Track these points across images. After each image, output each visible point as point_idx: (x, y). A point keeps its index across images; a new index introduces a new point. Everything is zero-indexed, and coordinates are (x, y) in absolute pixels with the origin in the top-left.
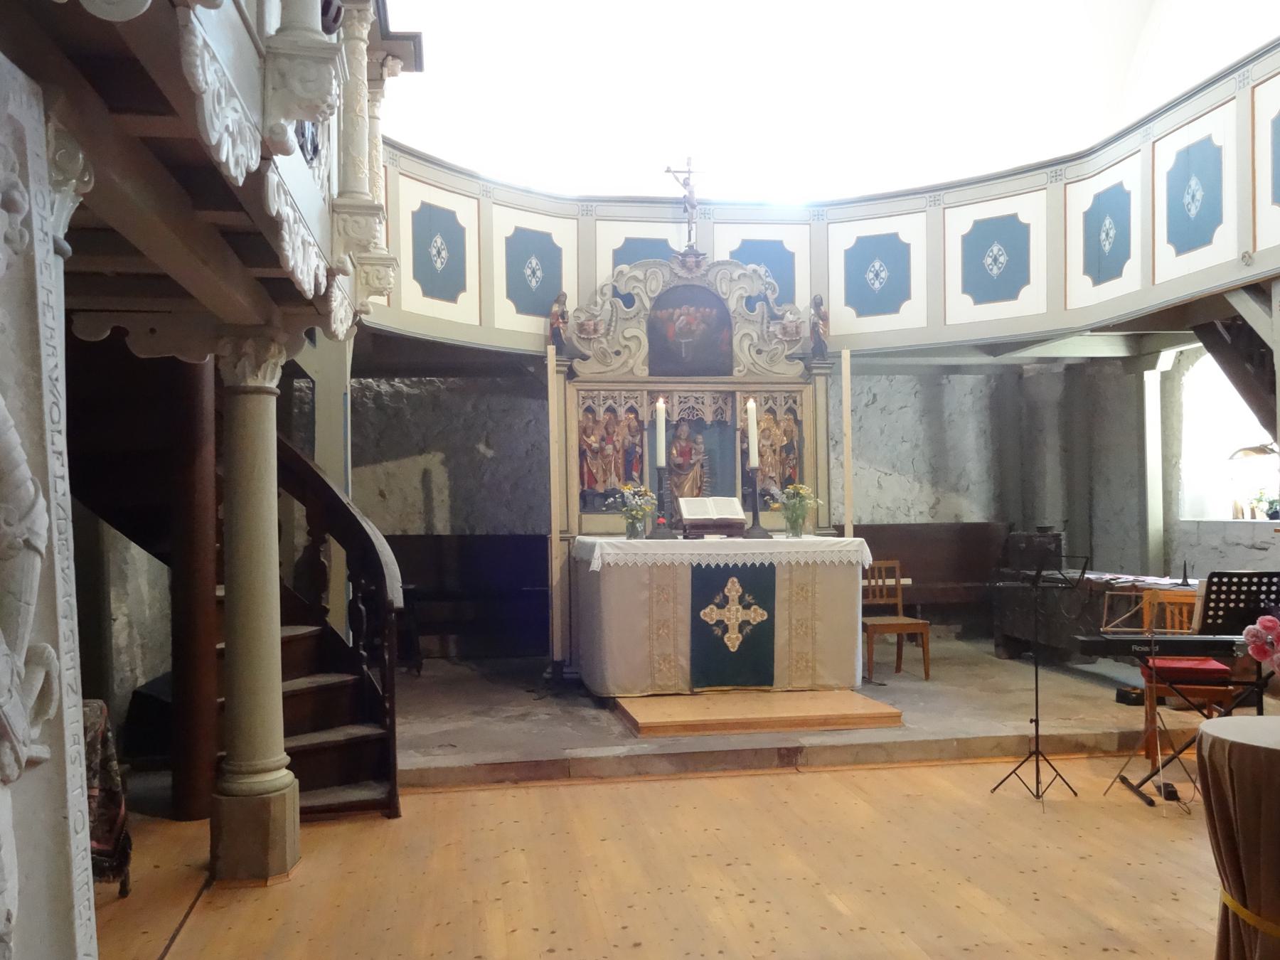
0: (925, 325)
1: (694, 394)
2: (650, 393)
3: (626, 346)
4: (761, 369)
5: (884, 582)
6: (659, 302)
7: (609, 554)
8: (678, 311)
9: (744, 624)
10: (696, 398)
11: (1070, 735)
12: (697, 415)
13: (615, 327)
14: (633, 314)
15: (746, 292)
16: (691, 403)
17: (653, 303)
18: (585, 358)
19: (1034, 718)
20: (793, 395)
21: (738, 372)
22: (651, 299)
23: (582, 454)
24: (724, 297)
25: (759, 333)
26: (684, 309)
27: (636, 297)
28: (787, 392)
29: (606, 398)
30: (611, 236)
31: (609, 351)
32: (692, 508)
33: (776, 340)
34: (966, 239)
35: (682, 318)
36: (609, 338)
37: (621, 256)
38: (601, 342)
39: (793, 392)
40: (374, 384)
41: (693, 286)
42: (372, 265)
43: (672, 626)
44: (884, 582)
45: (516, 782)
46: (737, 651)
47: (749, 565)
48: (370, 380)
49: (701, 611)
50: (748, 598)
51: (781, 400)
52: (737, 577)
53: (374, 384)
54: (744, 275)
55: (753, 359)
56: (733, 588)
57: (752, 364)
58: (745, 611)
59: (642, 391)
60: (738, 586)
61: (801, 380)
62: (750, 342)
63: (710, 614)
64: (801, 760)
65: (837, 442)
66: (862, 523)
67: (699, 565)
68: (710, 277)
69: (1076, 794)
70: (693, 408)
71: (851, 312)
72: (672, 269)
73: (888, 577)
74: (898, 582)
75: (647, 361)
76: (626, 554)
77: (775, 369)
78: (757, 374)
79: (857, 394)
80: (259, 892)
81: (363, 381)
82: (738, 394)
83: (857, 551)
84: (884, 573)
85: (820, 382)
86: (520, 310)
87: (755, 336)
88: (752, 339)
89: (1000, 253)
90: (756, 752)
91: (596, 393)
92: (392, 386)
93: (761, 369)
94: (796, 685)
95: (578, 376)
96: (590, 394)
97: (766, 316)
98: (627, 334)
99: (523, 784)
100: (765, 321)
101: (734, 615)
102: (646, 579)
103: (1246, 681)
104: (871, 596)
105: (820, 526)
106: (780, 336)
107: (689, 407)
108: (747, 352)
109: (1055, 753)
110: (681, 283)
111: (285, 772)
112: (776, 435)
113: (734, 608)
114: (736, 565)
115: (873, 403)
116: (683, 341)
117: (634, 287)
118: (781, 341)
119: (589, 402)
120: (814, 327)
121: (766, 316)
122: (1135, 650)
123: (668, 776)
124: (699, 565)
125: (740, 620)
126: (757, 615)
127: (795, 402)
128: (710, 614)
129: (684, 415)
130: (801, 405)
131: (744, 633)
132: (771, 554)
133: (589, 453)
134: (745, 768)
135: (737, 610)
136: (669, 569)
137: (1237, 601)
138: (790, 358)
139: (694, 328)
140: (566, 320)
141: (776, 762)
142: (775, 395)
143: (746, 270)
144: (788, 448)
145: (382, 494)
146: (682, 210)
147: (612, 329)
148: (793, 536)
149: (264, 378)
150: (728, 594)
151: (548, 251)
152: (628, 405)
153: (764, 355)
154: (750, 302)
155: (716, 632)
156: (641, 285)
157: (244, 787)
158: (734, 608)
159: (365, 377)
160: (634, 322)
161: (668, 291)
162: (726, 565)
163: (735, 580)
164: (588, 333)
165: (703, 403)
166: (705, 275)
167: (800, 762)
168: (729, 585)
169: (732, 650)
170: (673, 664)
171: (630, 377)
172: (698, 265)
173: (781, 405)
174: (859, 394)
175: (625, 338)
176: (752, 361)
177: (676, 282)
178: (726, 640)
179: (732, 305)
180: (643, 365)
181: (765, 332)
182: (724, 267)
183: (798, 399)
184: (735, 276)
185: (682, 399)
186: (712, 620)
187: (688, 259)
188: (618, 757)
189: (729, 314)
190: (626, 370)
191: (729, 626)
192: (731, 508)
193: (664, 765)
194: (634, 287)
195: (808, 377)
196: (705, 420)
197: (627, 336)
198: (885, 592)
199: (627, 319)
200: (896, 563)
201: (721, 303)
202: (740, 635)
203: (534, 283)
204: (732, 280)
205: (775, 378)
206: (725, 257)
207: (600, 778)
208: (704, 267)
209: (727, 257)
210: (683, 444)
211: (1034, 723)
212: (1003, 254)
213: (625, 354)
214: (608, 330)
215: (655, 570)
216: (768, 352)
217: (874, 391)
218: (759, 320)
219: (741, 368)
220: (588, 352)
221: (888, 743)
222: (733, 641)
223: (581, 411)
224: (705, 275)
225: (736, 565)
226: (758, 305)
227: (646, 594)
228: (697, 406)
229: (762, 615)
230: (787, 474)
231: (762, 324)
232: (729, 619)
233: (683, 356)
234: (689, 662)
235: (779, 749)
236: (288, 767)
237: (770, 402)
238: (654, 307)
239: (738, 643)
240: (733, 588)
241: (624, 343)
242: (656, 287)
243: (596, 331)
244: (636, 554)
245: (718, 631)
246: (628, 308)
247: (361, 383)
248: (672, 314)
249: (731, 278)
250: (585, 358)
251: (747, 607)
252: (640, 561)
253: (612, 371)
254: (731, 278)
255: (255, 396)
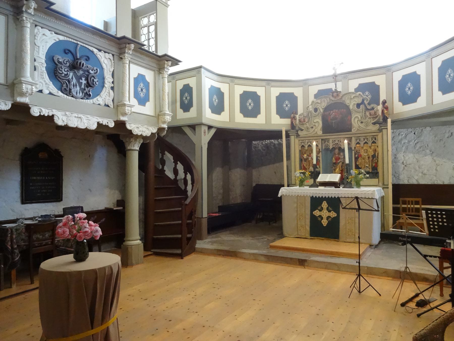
0: (426, 106)
1: (337, 139)
2: (322, 140)
3: (315, 125)
4: (362, 129)
5: (414, 206)
6: (326, 109)
7: (284, 192)
8: (332, 112)
9: (328, 218)
10: (338, 140)
11: (421, 274)
12: (339, 146)
13: (311, 119)
14: (317, 114)
15: (356, 102)
16: (337, 142)
17: (323, 110)
18: (302, 130)
19: (358, 261)
20: (375, 137)
21: (354, 130)
22: (323, 109)
23: (301, 160)
24: (348, 105)
25: (361, 116)
26: (334, 111)
27: (318, 109)
28: (372, 136)
29: (308, 142)
30: (313, 90)
31: (309, 127)
32: (322, 178)
33: (368, 118)
34: (440, 69)
35: (333, 114)
36: (309, 123)
37: (316, 96)
38: (307, 124)
39: (359, 137)
40: (274, 141)
41: (337, 103)
42: (162, 115)
43: (304, 216)
44: (414, 206)
45: (223, 256)
46: (326, 226)
47: (330, 197)
48: (272, 140)
49: (313, 211)
50: (330, 209)
51: (362, 139)
52: (326, 201)
53: (274, 141)
54: (356, 96)
55: (359, 125)
56: (325, 205)
57: (359, 127)
58: (329, 213)
59: (319, 139)
60: (326, 204)
61: (378, 131)
62: (358, 119)
63: (317, 213)
64: (306, 264)
65: (433, 152)
66: (445, 184)
67: (313, 196)
68: (343, 99)
69: (380, 295)
70: (337, 144)
71: (401, 104)
72: (330, 98)
73: (415, 204)
74: (421, 206)
75: (322, 129)
76: (289, 192)
77: (368, 128)
78: (361, 130)
79: (443, 133)
80: (126, 268)
81: (271, 141)
82: (353, 138)
83: (372, 194)
84: (414, 203)
85: (384, 131)
86: (281, 117)
87: (360, 117)
88: (359, 118)
89: (451, 72)
90: (291, 259)
91: (305, 141)
92: (278, 141)
93: (362, 129)
94: (348, 240)
95: (300, 136)
96: (303, 141)
97: (364, 110)
98: (315, 121)
99: (225, 257)
100: (364, 111)
101: (325, 214)
102: (296, 200)
103: (336, 251)
104: (407, 211)
105: (385, 184)
106: (369, 116)
107: (336, 144)
108: (356, 123)
109: (419, 281)
110: (333, 102)
111: (139, 241)
112: (370, 151)
113: (325, 212)
114: (325, 197)
115: (451, 136)
116: (334, 122)
117: (317, 106)
118: (370, 118)
119: (303, 144)
120: (383, 111)
121: (364, 110)
122: (400, 239)
123: (266, 262)
124: (313, 196)
125: (327, 216)
126: (333, 214)
127: (375, 139)
128: (317, 213)
129: (334, 146)
130: (378, 140)
131: (329, 220)
132: (338, 194)
133: (303, 160)
134: (287, 263)
135: (326, 212)
136: (304, 197)
137: (442, 222)
138: (374, 124)
139: (337, 117)
140: (295, 119)
141: (298, 263)
142: (367, 137)
143: (356, 94)
144: (374, 156)
145: (275, 173)
146: (332, 78)
147: (310, 120)
148: (357, 187)
149: (131, 147)
150: (323, 207)
151: (292, 98)
152: (308, 145)
153: (364, 123)
154: (358, 106)
155: (319, 219)
156: (319, 105)
157: (127, 244)
158: (325, 212)
159: (271, 139)
160: (317, 117)
161: (328, 106)
162: (322, 197)
163: (325, 202)
164: (302, 122)
165: (341, 142)
166: (342, 98)
167: (306, 265)
168: (323, 204)
169: (324, 226)
170: (304, 228)
171: (316, 135)
172: (338, 95)
173: (370, 141)
174: (444, 133)
175: (314, 122)
176: (358, 126)
177: (331, 102)
178: (322, 222)
179: (351, 107)
180: (320, 130)
181: (363, 115)
182: (348, 95)
183: (377, 138)
184: (352, 97)
185: (333, 141)
186: (317, 215)
187: (334, 94)
188: (250, 253)
189: (350, 110)
190: (314, 133)
191: (323, 217)
192: (336, 177)
193: (263, 258)
194: (317, 106)
195: (380, 131)
196: (342, 147)
197: (315, 122)
198: (414, 210)
199: (315, 116)
200: (420, 199)
201: (347, 107)
202: (327, 221)
203: (250, 108)
204: (351, 99)
205: (368, 131)
206: (353, 91)
207: (245, 259)
208: (341, 95)
209: (353, 91)
210: (337, 156)
211: (358, 263)
212: (452, 73)
213: (314, 128)
214: (309, 120)
215: (298, 197)
216: (365, 122)
217: (451, 131)
218: (362, 111)
219: (355, 129)
220: (303, 128)
221: (339, 264)
222: (325, 222)
223: (300, 147)
224: (342, 98)
225: (325, 197)
226: (361, 106)
227: (295, 205)
228: (338, 143)
229: (315, 213)
230: (374, 165)
231: (362, 112)
232: (323, 215)
233: (334, 126)
234: (309, 228)
235: (299, 259)
236: (140, 240)
237: (366, 140)
238: (324, 111)
239: (326, 223)
240: (325, 205)
241: (314, 124)
242: (324, 105)
243: (304, 121)
244: (292, 192)
245: (319, 219)
246: (315, 112)
247: (270, 141)
248: (330, 113)
249: (351, 98)
250: (302, 130)
251: (330, 211)
252: (293, 194)
253: (310, 133)
254: (351, 98)
255: (131, 151)
